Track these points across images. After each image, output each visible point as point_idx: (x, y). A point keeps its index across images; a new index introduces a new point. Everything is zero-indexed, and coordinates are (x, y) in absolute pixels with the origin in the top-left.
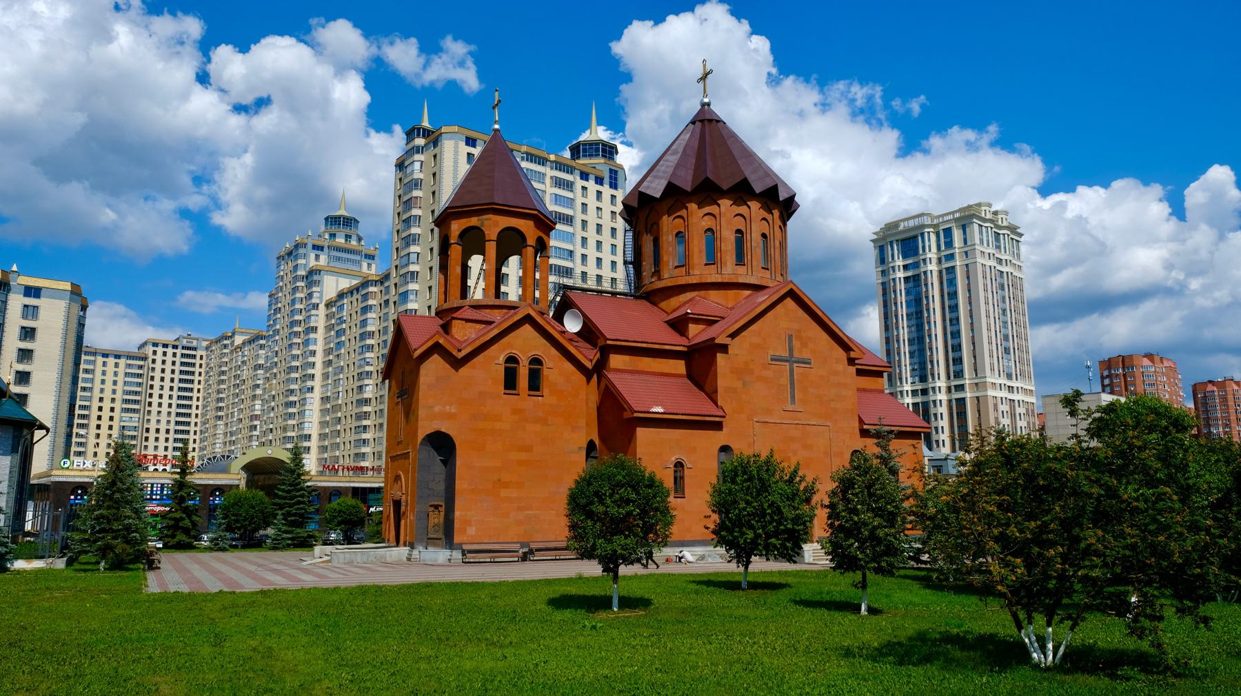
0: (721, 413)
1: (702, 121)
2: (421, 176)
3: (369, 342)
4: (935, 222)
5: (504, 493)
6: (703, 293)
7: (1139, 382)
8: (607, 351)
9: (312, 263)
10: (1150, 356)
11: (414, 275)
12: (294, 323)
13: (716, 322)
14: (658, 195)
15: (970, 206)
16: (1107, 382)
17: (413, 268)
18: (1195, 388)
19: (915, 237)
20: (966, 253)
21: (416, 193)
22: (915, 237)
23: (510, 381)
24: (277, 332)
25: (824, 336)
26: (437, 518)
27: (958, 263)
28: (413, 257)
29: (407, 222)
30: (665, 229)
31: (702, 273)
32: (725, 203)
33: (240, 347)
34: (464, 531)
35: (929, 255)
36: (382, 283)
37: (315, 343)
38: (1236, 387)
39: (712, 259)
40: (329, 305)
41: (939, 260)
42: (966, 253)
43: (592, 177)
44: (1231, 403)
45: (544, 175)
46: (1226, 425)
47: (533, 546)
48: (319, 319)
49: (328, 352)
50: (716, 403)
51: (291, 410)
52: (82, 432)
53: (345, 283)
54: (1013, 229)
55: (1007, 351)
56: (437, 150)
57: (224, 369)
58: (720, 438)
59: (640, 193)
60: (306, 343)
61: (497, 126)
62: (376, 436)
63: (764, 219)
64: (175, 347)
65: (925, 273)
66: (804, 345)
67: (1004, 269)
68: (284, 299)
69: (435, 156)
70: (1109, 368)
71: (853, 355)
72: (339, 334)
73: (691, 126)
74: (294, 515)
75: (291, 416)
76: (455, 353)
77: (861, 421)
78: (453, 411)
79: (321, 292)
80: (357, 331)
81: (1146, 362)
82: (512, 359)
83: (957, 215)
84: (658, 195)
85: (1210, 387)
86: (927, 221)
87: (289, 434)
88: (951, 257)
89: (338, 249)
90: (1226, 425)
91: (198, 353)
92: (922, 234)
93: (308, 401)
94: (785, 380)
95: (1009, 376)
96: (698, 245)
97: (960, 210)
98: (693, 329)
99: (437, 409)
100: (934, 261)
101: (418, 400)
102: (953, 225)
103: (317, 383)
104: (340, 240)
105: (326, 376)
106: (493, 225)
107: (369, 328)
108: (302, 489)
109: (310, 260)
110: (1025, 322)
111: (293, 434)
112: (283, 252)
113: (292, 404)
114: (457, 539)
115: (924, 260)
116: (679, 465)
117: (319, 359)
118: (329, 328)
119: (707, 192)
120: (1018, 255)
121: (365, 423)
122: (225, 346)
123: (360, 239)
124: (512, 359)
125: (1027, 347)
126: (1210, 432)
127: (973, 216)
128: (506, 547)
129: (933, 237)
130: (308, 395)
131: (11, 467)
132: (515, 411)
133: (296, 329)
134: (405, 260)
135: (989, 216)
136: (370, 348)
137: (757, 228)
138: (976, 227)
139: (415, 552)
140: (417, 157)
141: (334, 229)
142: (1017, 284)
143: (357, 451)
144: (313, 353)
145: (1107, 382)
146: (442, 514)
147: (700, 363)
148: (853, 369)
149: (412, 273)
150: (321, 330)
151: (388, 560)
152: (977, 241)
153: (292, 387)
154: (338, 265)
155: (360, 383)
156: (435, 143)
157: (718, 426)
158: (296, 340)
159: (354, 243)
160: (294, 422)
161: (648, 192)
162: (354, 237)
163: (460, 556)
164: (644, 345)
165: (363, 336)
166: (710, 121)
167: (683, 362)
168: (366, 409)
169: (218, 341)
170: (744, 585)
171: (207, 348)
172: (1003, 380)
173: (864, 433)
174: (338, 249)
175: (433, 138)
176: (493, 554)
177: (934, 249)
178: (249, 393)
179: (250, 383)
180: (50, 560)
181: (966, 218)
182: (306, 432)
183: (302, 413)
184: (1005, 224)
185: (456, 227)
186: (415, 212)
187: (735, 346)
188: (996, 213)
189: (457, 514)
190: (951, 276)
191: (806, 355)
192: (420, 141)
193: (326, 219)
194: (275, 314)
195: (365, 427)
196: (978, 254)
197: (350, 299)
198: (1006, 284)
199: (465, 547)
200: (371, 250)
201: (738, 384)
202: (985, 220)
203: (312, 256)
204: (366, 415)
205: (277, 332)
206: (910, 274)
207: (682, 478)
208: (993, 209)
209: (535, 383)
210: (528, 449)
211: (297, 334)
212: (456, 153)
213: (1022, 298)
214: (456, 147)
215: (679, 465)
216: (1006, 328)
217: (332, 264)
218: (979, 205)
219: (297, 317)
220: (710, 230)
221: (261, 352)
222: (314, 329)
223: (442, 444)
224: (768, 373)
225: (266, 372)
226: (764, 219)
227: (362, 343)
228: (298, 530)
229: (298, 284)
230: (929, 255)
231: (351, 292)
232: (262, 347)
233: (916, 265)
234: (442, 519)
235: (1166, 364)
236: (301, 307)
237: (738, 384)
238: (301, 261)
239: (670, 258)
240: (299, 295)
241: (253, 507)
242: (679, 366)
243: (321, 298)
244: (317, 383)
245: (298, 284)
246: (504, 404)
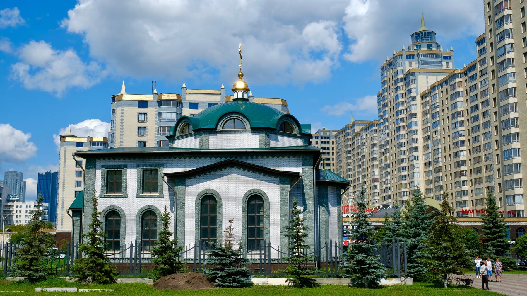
3: (460, 119)
9: (407, 68)
11: (511, 61)
12: (399, 113)
17: (509, 56)
29: (500, 22)
33: (359, 134)
40: (423, 96)
48: (417, 107)
49: (426, 130)
51: (403, 173)
52: (18, 214)
53: (433, 79)
57: (349, 149)
60: (410, 125)
62: (473, 188)
64: (317, 138)
68: (389, 96)
72: (434, 116)
75: (403, 177)
79: (416, 88)
80: (449, 113)
87: (404, 190)
89: (425, 55)
91: (331, 140)
93: (416, 166)
103: (420, 153)
105: (426, 147)
107: (459, 109)
108: (500, 226)
109: (406, 66)
112: (383, 62)
113: (404, 169)
117: (420, 136)
118: (425, 113)
122: (348, 134)
123: (438, 46)
131: (196, 214)
133: (401, 116)
136: (461, 123)
143: (459, 200)
144: (415, 132)
149: (509, 60)
150: (419, 115)
153: (402, 157)
158: (402, 124)
159: (434, 49)
160: (406, 182)
162: (434, 45)
165: (454, 116)
168: (462, 168)
169: (343, 131)
171: (336, 137)
174: (425, 55)
178: (370, 164)
179: (370, 157)
180: (403, 279)
194: (384, 107)
195: (463, 182)
197: (440, 90)
200: (447, 52)
203: (407, 63)
204: (463, 173)
205: (386, 120)
211: (402, 120)
217: (421, 67)
219: (401, 108)
221: (375, 135)
222: (415, 115)
225: (381, 148)
227: (455, 121)
229: (399, 84)
231: (441, 84)
232: (375, 131)
236: (403, 100)
238: (400, 68)
240: (400, 92)
243: (417, 92)
244: (420, 153)
245: (399, 84)
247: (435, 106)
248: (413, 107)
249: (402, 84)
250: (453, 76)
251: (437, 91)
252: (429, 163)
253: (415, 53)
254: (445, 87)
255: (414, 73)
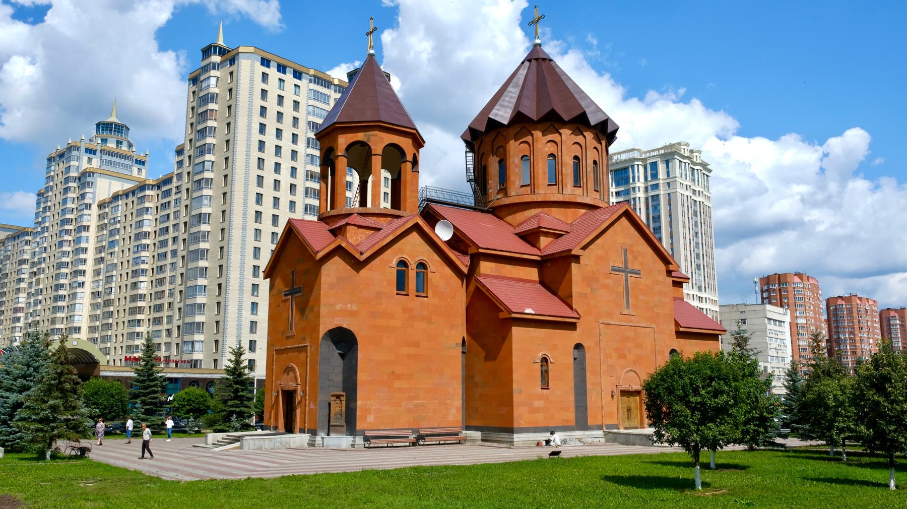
0: (577, 316)
1: (530, 61)
2: (217, 91)
3: (145, 241)
4: (644, 156)
5: (397, 384)
6: (546, 210)
7: (791, 295)
8: (476, 258)
9: (85, 165)
10: (799, 275)
11: (209, 181)
12: (64, 222)
13: (562, 235)
14: (506, 122)
15: (672, 146)
16: (765, 295)
17: (207, 175)
18: (829, 302)
19: (626, 169)
20: (669, 184)
21: (211, 106)
22: (626, 169)
23: (401, 284)
24: (46, 229)
25: (649, 250)
26: (338, 407)
27: (662, 191)
28: (208, 165)
29: (202, 133)
30: (512, 153)
31: (545, 192)
32: (566, 132)
34: (364, 419)
35: (638, 185)
36: (159, 187)
37: (87, 241)
38: (859, 302)
39: (555, 181)
40: (101, 206)
41: (646, 189)
42: (669, 184)
43: (274, 65)
44: (855, 315)
45: (329, 96)
46: (851, 333)
47: (423, 432)
48: (92, 218)
49: (99, 250)
50: (571, 307)
51: (60, 304)
53: (118, 186)
54: (704, 165)
55: (698, 267)
56: (233, 68)
58: (574, 337)
59: (490, 120)
60: (78, 240)
61: (372, 52)
63: (595, 148)
65: (634, 199)
66: (635, 258)
67: (698, 199)
69: (231, 73)
70: (768, 284)
71: (671, 267)
72: (112, 233)
73: (527, 64)
74: (150, 404)
76: (357, 256)
77: (677, 324)
78: (354, 308)
81: (797, 279)
82: (403, 263)
83: (662, 152)
84: (506, 122)
85: (840, 302)
86: (637, 155)
88: (656, 187)
89: (110, 153)
90: (851, 333)
92: (633, 166)
93: (79, 295)
94: (621, 288)
95: (700, 289)
96: (542, 168)
97: (664, 148)
98: (544, 241)
99: (338, 307)
100: (642, 189)
101: (318, 298)
102: (658, 160)
103: (88, 279)
104: (111, 145)
105: (97, 273)
106: (379, 141)
107: (145, 229)
108: (156, 379)
110: (712, 244)
111: (62, 326)
112: (53, 153)
114: (359, 426)
115: (634, 188)
116: (545, 360)
117: (90, 256)
118: (101, 228)
119: (551, 121)
120: (708, 187)
121: (139, 317)
123: (130, 146)
124: (403, 263)
125: (713, 264)
126: (839, 338)
127: (675, 153)
128: (401, 433)
129: (642, 169)
130: (79, 290)
132: (406, 310)
133: (67, 227)
134: (200, 168)
135: (687, 154)
136: (145, 247)
137: (592, 155)
138: (677, 162)
139: (318, 439)
140: (213, 73)
141: (105, 134)
142: (707, 211)
145: (765, 295)
146: (344, 403)
147: (554, 271)
148: (670, 280)
149: (207, 180)
151: (292, 446)
152: (678, 174)
154: (111, 168)
155: (134, 280)
156: (232, 61)
157: (572, 326)
158: (66, 238)
159: (124, 148)
160: (63, 315)
161: (497, 119)
163: (362, 442)
164: (508, 254)
165: (138, 236)
166: (544, 59)
167: (536, 270)
170: (712, 466)
172: (695, 292)
173: (680, 334)
174: (110, 153)
175: (230, 57)
176: (390, 440)
177: (642, 179)
179: (15, 277)
181: (669, 154)
182: (75, 325)
183: (71, 307)
184: (698, 161)
185: (343, 141)
186: (210, 123)
187: (587, 257)
188: (692, 151)
189: (359, 403)
190: (655, 203)
191: (636, 266)
192: (216, 59)
193: (98, 125)
195: (139, 321)
196: (678, 185)
197: (125, 201)
198: (699, 211)
199: (367, 433)
201: (587, 290)
202: (684, 157)
203: (85, 158)
204: (140, 310)
205: (46, 229)
206: (621, 199)
207: (547, 371)
208: (690, 148)
209: (422, 287)
210: (416, 344)
211: (68, 232)
212: (252, 72)
213: (710, 223)
214: (252, 67)
215: (545, 360)
216: (698, 248)
217: (104, 167)
218: (680, 144)
219: (68, 216)
220: (552, 155)
222: (86, 228)
223: (344, 340)
224: (609, 281)
226: (595, 148)
228: (153, 418)
229: (70, 184)
230: (638, 185)
231: (126, 194)
232: (28, 243)
233: (627, 192)
234: (344, 408)
235: (811, 281)
236: (73, 206)
237: (587, 290)
238: (74, 163)
239: (518, 174)
240: (71, 195)
241: (113, 396)
242: (532, 273)
243: (94, 198)
244: (88, 279)
245: (70, 184)
246: (395, 303)
247: (115, 221)
248: (85, 217)
249: (75, 185)
250: (143, 187)
251: (120, 202)
252: (98, 293)
253: (99, 148)
254: (131, 198)
255: (94, 173)
